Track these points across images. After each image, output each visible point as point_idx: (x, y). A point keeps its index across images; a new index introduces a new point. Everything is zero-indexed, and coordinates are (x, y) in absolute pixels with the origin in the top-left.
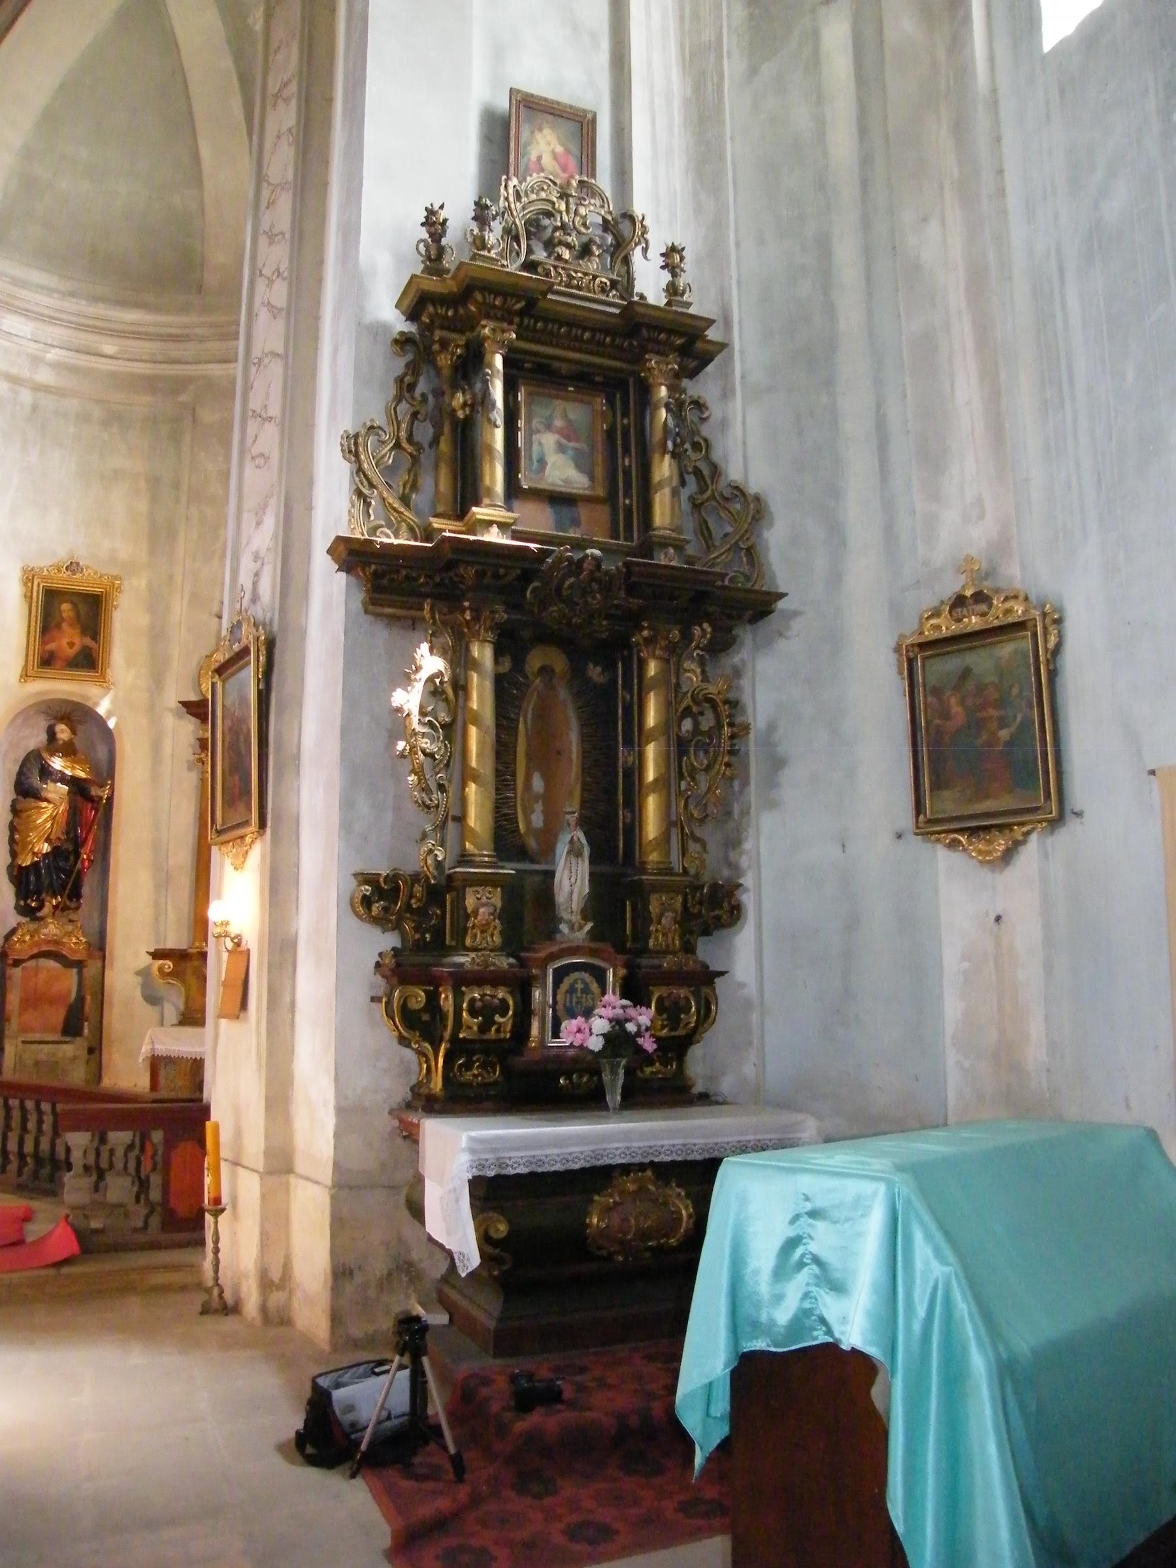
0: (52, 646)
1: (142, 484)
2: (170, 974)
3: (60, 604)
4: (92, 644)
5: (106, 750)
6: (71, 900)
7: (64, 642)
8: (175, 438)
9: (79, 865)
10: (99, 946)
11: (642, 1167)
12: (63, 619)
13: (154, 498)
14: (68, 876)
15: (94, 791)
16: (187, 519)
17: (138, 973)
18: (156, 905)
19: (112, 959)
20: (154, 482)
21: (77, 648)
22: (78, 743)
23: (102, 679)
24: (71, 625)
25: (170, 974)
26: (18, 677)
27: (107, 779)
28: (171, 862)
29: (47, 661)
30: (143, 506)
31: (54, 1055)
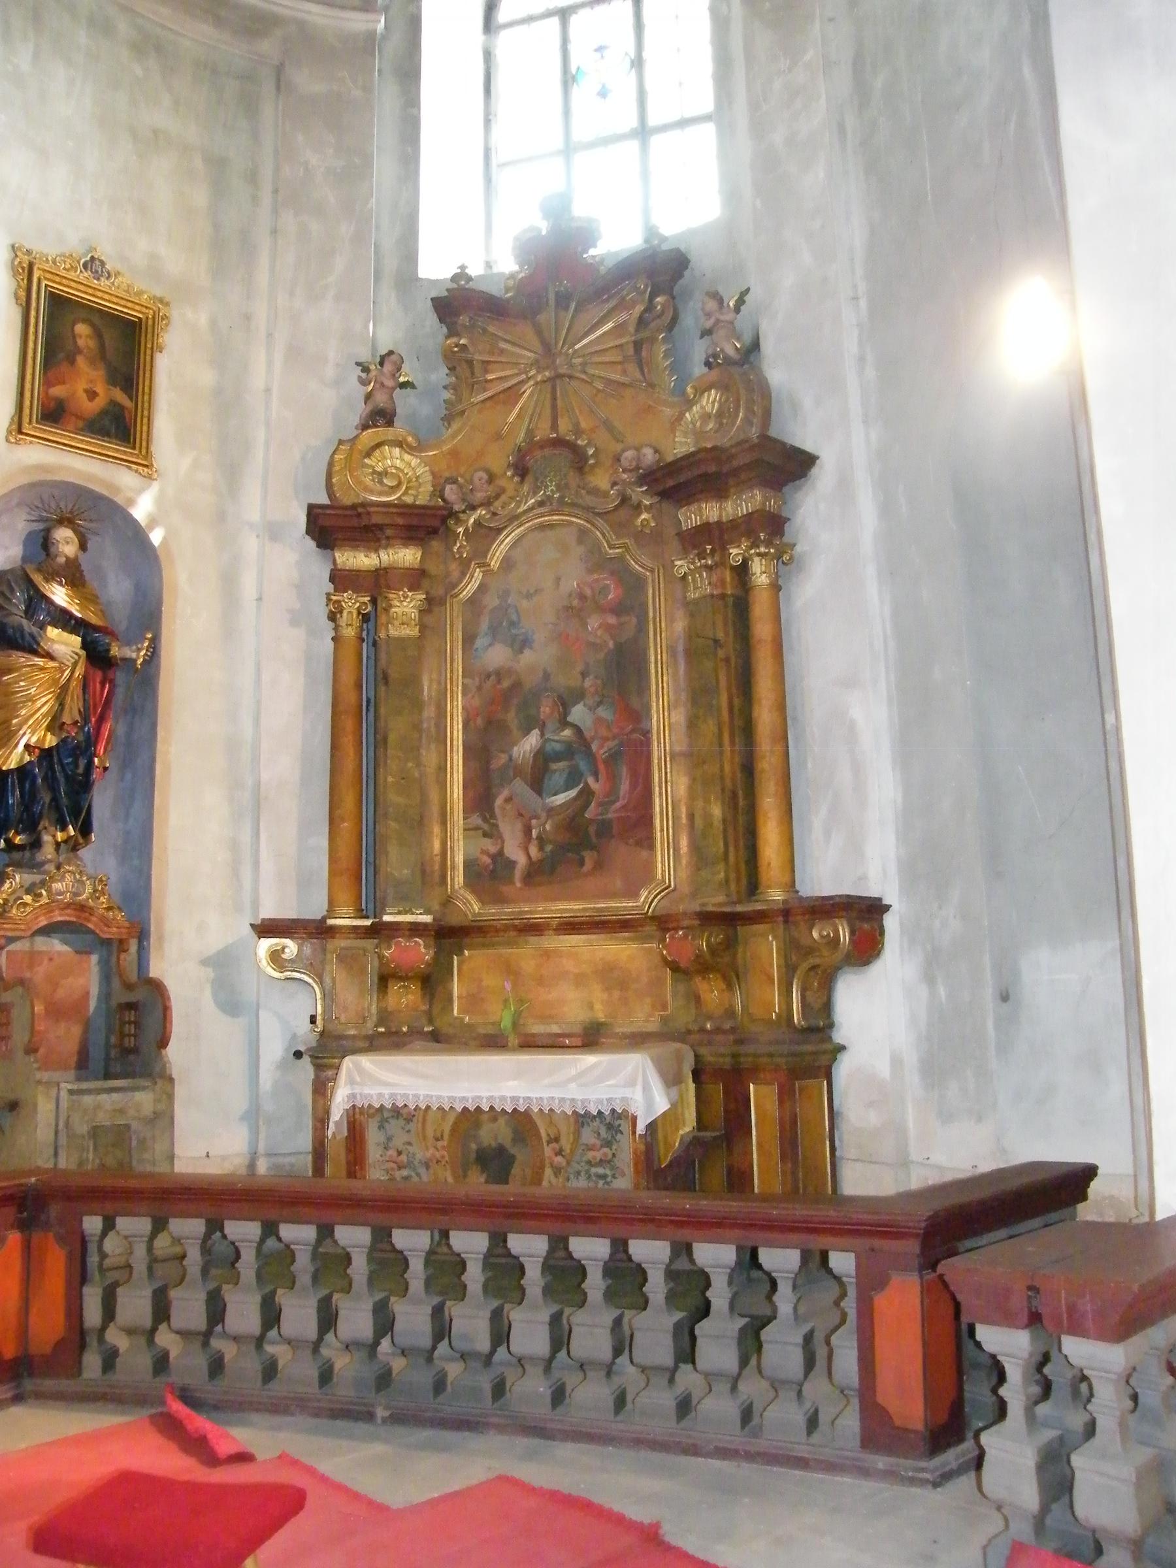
0: (57, 391)
1: (198, 163)
8: (249, 105)
12: (79, 351)
13: (219, 188)
16: (274, 232)
17: (205, 962)
18: (234, 846)
20: (218, 165)
21: (100, 403)
23: (144, 463)
24: (92, 362)
27: (148, 629)
29: (54, 414)
30: (200, 197)
31: (122, 1111)
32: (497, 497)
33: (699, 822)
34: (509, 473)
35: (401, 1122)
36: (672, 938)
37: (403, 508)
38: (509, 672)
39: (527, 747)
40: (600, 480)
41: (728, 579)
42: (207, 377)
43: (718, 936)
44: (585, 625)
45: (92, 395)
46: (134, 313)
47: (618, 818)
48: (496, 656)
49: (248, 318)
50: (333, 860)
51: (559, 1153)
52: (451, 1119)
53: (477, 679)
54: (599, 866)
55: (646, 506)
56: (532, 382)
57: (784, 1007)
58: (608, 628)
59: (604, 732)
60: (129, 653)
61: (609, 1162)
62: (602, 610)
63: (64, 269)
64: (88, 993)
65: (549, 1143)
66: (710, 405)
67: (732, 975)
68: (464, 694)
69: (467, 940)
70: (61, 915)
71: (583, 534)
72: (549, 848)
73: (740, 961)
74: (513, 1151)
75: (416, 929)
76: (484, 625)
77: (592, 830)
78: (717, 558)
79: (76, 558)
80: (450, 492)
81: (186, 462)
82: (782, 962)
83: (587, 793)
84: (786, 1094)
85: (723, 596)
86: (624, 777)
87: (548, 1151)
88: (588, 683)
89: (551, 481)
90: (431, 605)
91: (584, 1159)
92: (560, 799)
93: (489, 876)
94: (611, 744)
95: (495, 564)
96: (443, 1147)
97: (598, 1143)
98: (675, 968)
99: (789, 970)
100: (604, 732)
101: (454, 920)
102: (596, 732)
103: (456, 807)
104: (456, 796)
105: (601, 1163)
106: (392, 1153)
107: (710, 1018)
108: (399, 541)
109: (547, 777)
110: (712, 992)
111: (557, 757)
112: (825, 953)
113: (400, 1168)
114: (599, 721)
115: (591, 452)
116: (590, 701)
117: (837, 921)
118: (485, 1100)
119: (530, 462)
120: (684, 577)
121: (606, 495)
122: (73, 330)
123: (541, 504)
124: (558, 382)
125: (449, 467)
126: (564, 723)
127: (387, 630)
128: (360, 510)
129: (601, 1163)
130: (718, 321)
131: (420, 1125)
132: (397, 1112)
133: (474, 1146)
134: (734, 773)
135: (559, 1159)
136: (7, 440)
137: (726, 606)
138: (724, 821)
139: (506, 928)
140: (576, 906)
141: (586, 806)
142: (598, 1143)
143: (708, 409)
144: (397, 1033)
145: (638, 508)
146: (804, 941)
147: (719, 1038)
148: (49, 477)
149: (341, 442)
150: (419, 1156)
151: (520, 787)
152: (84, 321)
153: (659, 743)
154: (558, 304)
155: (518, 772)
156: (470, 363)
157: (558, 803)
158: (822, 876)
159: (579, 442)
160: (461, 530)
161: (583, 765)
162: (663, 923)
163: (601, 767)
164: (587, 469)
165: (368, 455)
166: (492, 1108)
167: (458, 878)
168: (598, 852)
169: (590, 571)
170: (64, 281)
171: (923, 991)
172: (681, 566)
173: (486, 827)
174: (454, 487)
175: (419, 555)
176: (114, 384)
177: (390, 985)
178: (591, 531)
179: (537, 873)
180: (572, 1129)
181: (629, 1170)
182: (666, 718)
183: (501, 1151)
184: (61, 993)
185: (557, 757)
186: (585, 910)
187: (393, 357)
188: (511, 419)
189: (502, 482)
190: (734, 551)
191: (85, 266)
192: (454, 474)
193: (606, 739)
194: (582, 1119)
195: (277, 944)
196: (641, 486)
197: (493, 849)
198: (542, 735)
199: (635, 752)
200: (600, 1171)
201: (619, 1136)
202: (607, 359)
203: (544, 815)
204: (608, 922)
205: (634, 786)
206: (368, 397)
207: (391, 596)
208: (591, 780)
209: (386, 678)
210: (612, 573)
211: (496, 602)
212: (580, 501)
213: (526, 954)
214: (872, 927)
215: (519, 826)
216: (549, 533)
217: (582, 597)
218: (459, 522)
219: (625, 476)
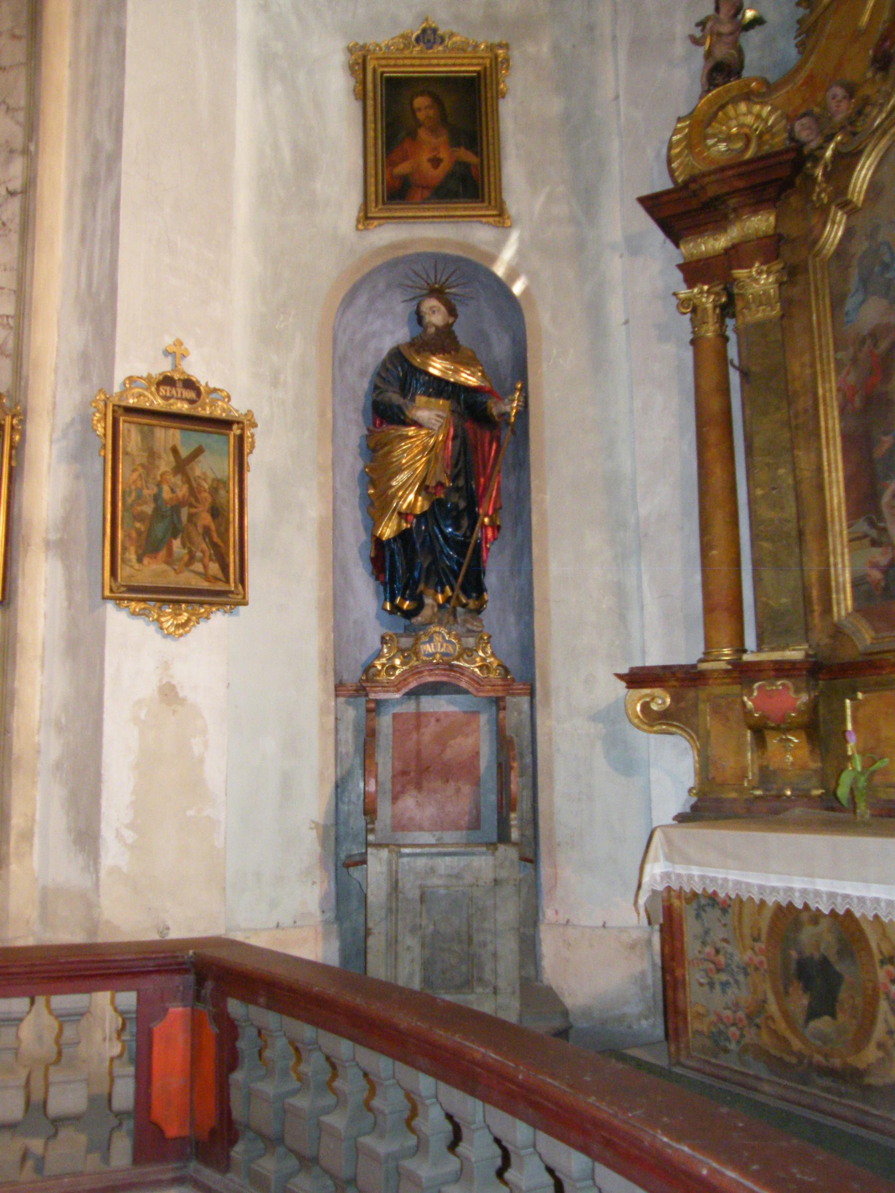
0: (403, 169)
4: (472, 159)
5: (507, 341)
6: (469, 597)
7: (424, 157)
9: (478, 533)
10: (520, 678)
11: (556, 882)
12: (419, 124)
14: (462, 554)
15: (496, 408)
17: (594, 718)
19: (547, 695)
24: (433, 131)
26: (353, 222)
42: (555, 106)
46: (469, 69)
49: (591, 28)
52: (767, 914)
63: (397, 50)
64: (478, 753)
68: (838, 372)
70: (430, 675)
75: (782, 669)
90: (792, 275)
96: (761, 950)
106: (709, 949)
113: (719, 970)
118: (797, 894)
122: (411, 105)
128: (693, 186)
131: (736, 919)
132: (713, 898)
133: (794, 954)
136: (357, 229)
148: (401, 253)
150: (736, 958)
152: (422, 94)
160: (819, 172)
166: (806, 906)
167: (844, 603)
170: (400, 62)
173: (873, 533)
175: (772, 219)
176: (458, 145)
183: (825, 962)
184: (449, 754)
189: (867, 90)
191: (418, 40)
206: (708, 55)
211: (865, 245)
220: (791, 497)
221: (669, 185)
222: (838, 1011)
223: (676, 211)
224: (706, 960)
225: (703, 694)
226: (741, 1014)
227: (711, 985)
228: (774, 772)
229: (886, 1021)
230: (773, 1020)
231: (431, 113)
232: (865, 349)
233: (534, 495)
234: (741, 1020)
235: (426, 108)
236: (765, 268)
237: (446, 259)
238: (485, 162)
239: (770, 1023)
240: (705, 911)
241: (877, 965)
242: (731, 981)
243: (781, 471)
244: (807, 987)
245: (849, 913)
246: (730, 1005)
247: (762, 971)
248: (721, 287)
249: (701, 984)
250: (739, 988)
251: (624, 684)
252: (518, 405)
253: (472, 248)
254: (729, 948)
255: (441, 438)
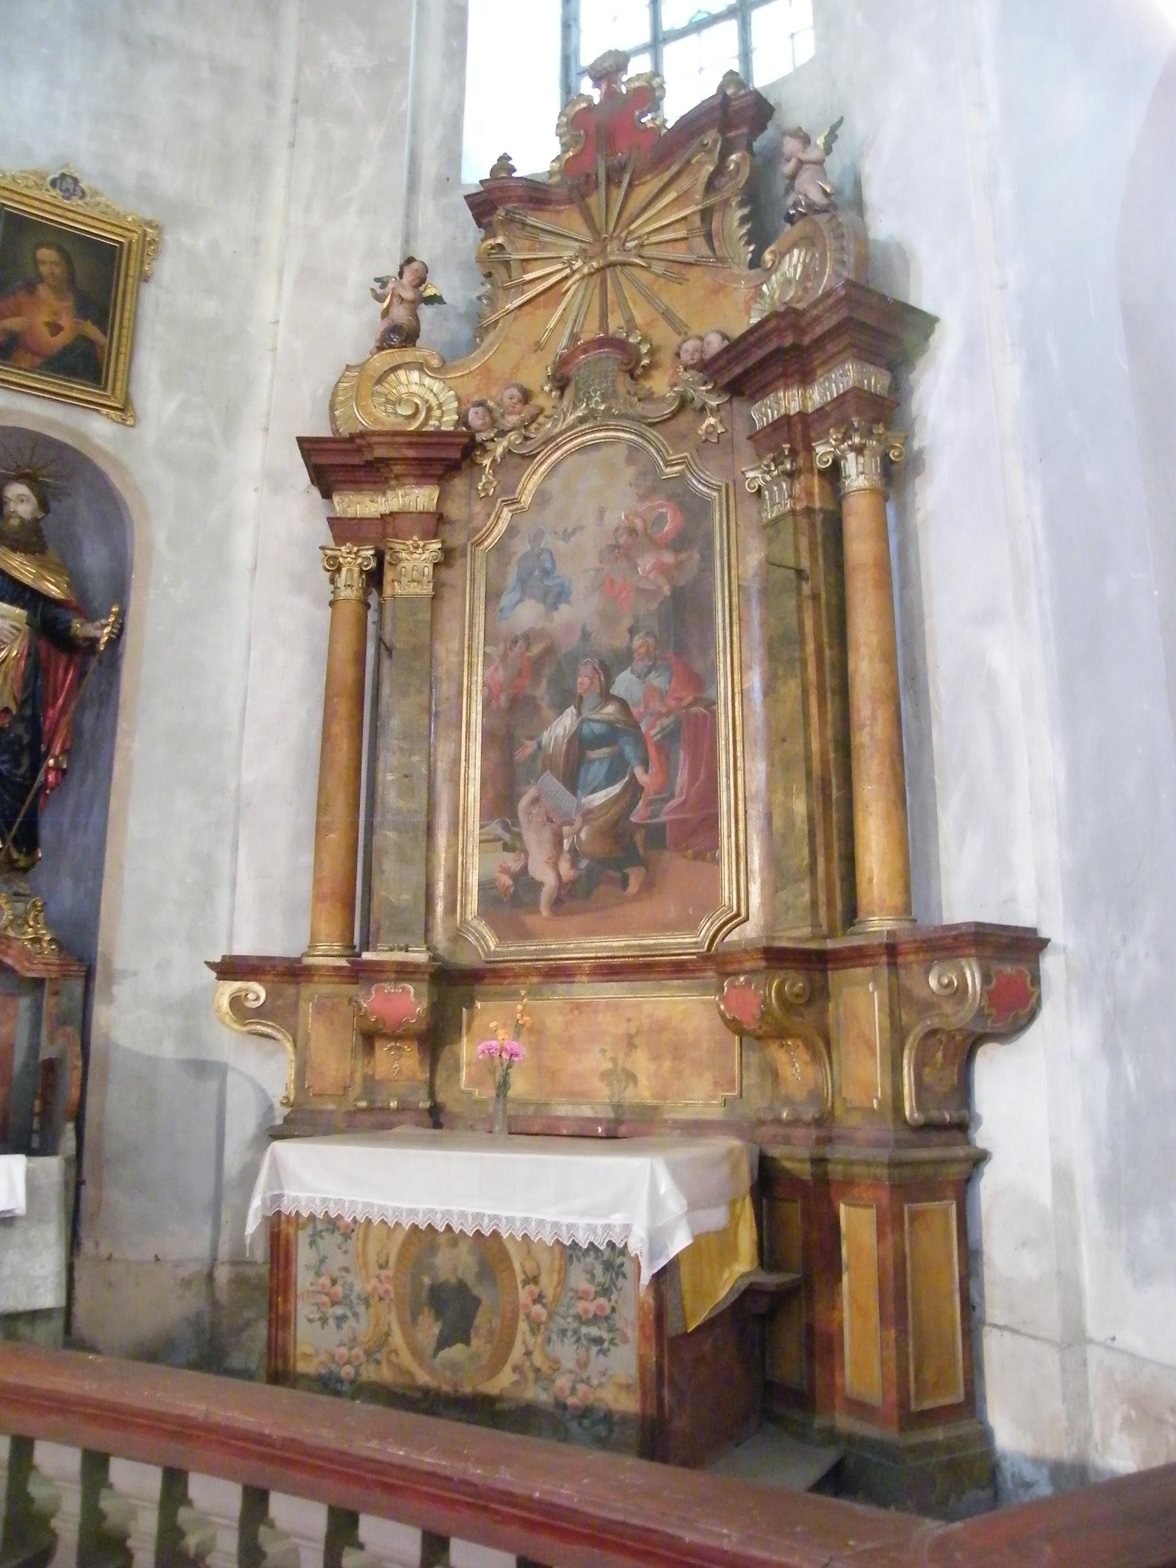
2: (260, 1013)
3: (38, 246)
6: (20, 852)
9: (40, 778)
12: (40, 279)
15: (79, 628)
22: (50, 527)
25: (260, 1013)
28: (249, 776)
32: (533, 419)
33: (778, 823)
34: (547, 388)
35: (337, 1238)
36: (732, 986)
37: (421, 439)
38: (541, 634)
39: (560, 731)
40: (659, 384)
41: (816, 489)
43: (796, 983)
44: (635, 566)
45: (56, 329)
46: (111, 235)
47: (677, 821)
48: (526, 614)
49: (257, 241)
50: (317, 881)
51: (539, 1299)
52: (400, 1237)
53: (502, 647)
54: (649, 886)
55: (711, 410)
56: (577, 276)
57: (889, 1091)
58: (662, 568)
59: (656, 705)
60: (90, 630)
61: (607, 1318)
62: (658, 545)
64: (12, 1046)
65: (525, 1283)
66: (792, 270)
67: (823, 1045)
69: (478, 988)
71: (634, 451)
72: (584, 863)
73: (831, 1020)
74: (478, 1291)
75: (404, 971)
76: (512, 578)
77: (639, 838)
78: (801, 461)
79: (36, 521)
80: (475, 418)
81: (171, 407)
82: (887, 1023)
83: (634, 788)
84: (890, 1223)
85: (809, 511)
86: (681, 762)
87: (524, 1295)
88: (637, 643)
89: (595, 391)
90: (447, 559)
91: (572, 1312)
92: (600, 798)
93: (509, 901)
94: (666, 721)
95: (526, 499)
96: (387, 1278)
97: (592, 1288)
98: (735, 1026)
99: (898, 1033)
100: (656, 705)
101: (465, 959)
102: (646, 706)
103: (470, 812)
104: (471, 797)
105: (595, 1320)
106: (325, 1280)
107: (788, 1101)
108: (411, 480)
109: (583, 771)
110: (795, 1068)
111: (598, 742)
112: (948, 1008)
113: (334, 1304)
114: (651, 693)
115: (644, 349)
116: (639, 665)
117: (963, 962)
118: (439, 1216)
119: (571, 370)
120: (759, 491)
121: (663, 399)
123: (582, 420)
124: (609, 272)
125: (478, 390)
126: (606, 696)
127: (394, 588)
129: (595, 1320)
130: (801, 163)
131: (360, 1243)
132: (333, 1224)
133: (427, 1280)
134: (824, 753)
135: (537, 1308)
137: (813, 525)
138: (810, 818)
139: (528, 972)
140: (618, 942)
141: (632, 805)
142: (592, 1288)
143: (790, 273)
144: (385, 1109)
145: (702, 410)
146: (919, 992)
147: (799, 1132)
149: (348, 368)
150: (357, 1289)
151: (551, 783)
152: (49, 245)
153: (727, 717)
154: (609, 180)
155: (549, 764)
156: (507, 264)
157: (597, 803)
158: (961, 901)
159: (631, 340)
160: (487, 462)
161: (629, 751)
162: (715, 964)
163: (652, 752)
164: (639, 371)
165: (380, 381)
166: (449, 1228)
168: (646, 868)
169: (643, 498)
171: (1102, 1070)
172: (755, 476)
173: (507, 837)
174: (480, 409)
176: (86, 318)
177: (377, 1044)
178: (644, 448)
179: (568, 898)
180: (557, 1264)
181: (633, 1334)
182: (742, 687)
183: (462, 1288)
185: (598, 742)
186: (629, 947)
187: (414, 265)
188: (552, 324)
189: (540, 401)
190: (820, 450)
191: (54, 183)
192: (484, 398)
193: (660, 715)
194: (570, 1252)
195: (240, 990)
196: (705, 384)
197: (515, 866)
198: (579, 714)
199: (696, 732)
200: (594, 1331)
201: (620, 1282)
202: (673, 236)
203: (578, 820)
204: (659, 964)
205: (693, 775)
206: (386, 313)
207: (398, 547)
208: (638, 771)
209: (389, 650)
210: (671, 497)
212: (631, 411)
213: (552, 1008)
214: (1020, 973)
215: (547, 834)
216: (595, 455)
217: (632, 532)
218: (485, 451)
219: (687, 375)
220: (424, 787)
221: (326, 432)
222: (472, 1335)
223: (336, 463)
224: (318, 1292)
225: (306, 990)
226: (358, 1351)
227: (324, 1321)
228: (381, 1082)
229: (524, 1342)
230: (396, 1352)
231: (58, 270)
232: (516, 650)
233: (119, 739)
234: (357, 1357)
235: (52, 263)
236: (421, 543)
237: (50, 442)
238: (114, 345)
239: (393, 1357)
240: (322, 1237)
241: (520, 1286)
242: (349, 1314)
243: (415, 758)
244: (439, 1314)
245: (495, 1234)
246: (346, 1342)
247: (387, 1300)
248: (372, 552)
249: (311, 1321)
250: (358, 1321)
251: (214, 975)
252: (111, 632)
253: (84, 438)
254: (350, 1278)
255: (14, 653)
